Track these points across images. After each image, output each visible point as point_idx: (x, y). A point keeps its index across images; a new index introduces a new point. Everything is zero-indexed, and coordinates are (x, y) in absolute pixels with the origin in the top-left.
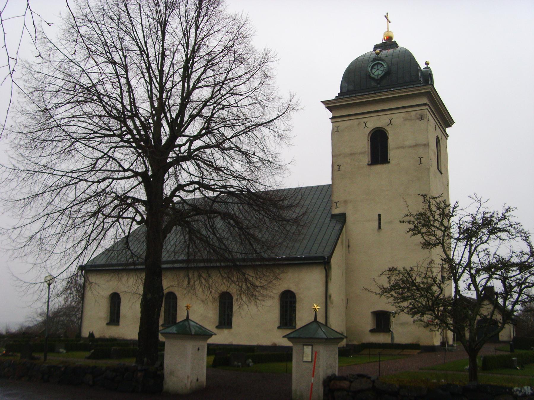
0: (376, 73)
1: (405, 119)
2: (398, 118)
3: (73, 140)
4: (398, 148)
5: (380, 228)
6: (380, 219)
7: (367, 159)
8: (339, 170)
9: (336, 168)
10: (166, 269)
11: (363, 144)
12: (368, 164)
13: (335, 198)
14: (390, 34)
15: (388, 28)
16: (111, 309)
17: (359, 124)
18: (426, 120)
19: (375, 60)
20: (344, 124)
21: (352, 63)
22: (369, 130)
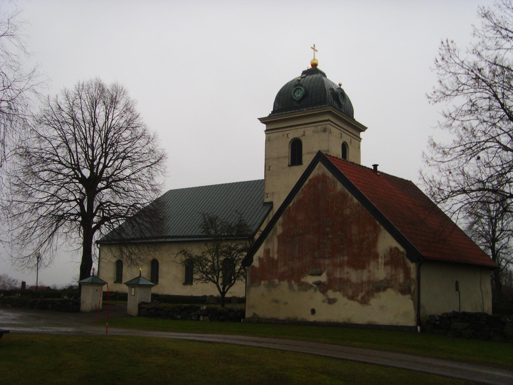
0: (297, 96)
1: (314, 132)
2: (309, 130)
3: (58, 200)
8: (269, 170)
9: (268, 168)
11: (286, 150)
12: (289, 166)
13: (266, 191)
14: (315, 62)
15: (314, 56)
16: (117, 272)
17: (283, 135)
18: (327, 132)
20: (274, 135)
21: (283, 87)
22: (289, 140)
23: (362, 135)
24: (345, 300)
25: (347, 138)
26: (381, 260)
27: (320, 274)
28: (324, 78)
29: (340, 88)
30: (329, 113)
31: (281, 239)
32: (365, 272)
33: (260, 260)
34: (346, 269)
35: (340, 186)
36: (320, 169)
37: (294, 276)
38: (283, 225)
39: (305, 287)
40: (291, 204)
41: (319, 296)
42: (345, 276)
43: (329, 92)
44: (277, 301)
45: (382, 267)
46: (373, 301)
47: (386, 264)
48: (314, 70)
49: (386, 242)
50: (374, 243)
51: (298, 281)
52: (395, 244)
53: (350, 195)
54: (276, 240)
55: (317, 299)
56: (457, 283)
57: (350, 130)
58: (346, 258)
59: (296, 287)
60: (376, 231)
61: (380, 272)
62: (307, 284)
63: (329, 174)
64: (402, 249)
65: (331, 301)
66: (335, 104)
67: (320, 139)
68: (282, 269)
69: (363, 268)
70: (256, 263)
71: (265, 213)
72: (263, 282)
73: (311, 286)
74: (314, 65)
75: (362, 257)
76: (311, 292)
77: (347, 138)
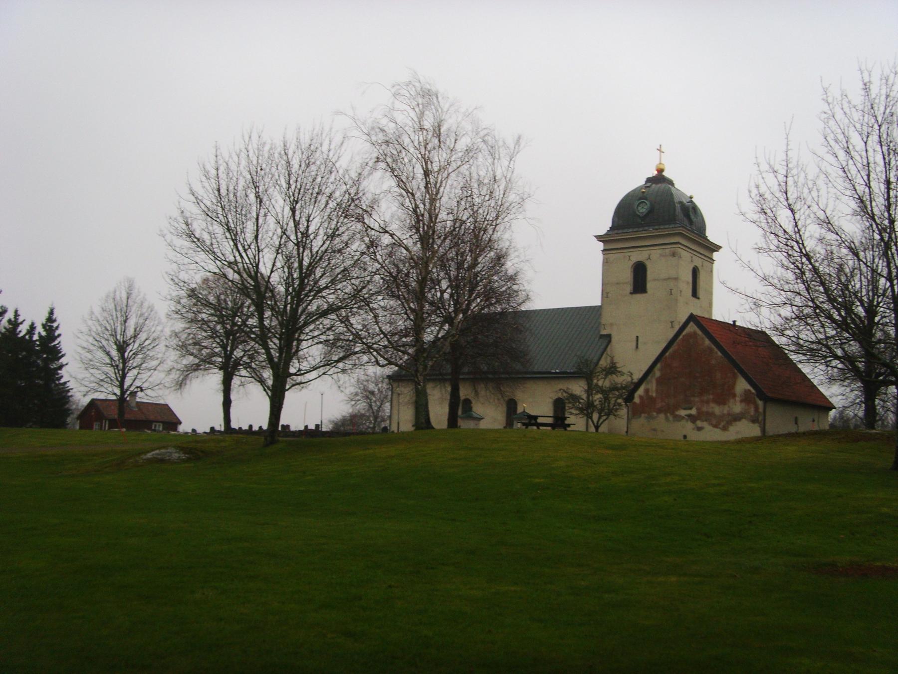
1: (661, 255)
2: (656, 253)
4: (654, 280)
5: (637, 347)
6: (637, 341)
7: (629, 288)
10: (463, 379)
11: (627, 275)
13: (603, 321)
14: (661, 167)
17: (625, 257)
19: (640, 199)
20: (613, 256)
21: (622, 201)
22: (631, 263)
23: (716, 255)
24: (710, 428)
25: (698, 262)
26: (738, 399)
27: (691, 409)
28: (672, 188)
29: (692, 202)
30: (680, 234)
31: (659, 381)
32: (726, 407)
33: (641, 397)
34: (712, 405)
35: (707, 342)
36: (692, 328)
37: (670, 410)
38: (661, 370)
39: (679, 418)
40: (667, 354)
41: (689, 425)
42: (710, 410)
43: (678, 206)
44: (655, 430)
45: (738, 404)
46: (731, 428)
47: (741, 401)
48: (659, 178)
49: (742, 385)
50: (733, 386)
51: (673, 413)
52: (748, 387)
53: (716, 350)
54: (654, 382)
55: (688, 428)
56: (796, 418)
57: (702, 251)
58: (711, 397)
59: (671, 418)
60: (735, 377)
61: (737, 407)
62: (680, 416)
63: (699, 332)
64: (753, 391)
65: (699, 429)
66: (686, 222)
67: (666, 264)
68: (659, 405)
69: (724, 404)
70: (637, 400)
71: (602, 347)
72: (643, 415)
73: (683, 418)
74: (660, 171)
75: (724, 395)
76: (683, 422)
77: (698, 262)
